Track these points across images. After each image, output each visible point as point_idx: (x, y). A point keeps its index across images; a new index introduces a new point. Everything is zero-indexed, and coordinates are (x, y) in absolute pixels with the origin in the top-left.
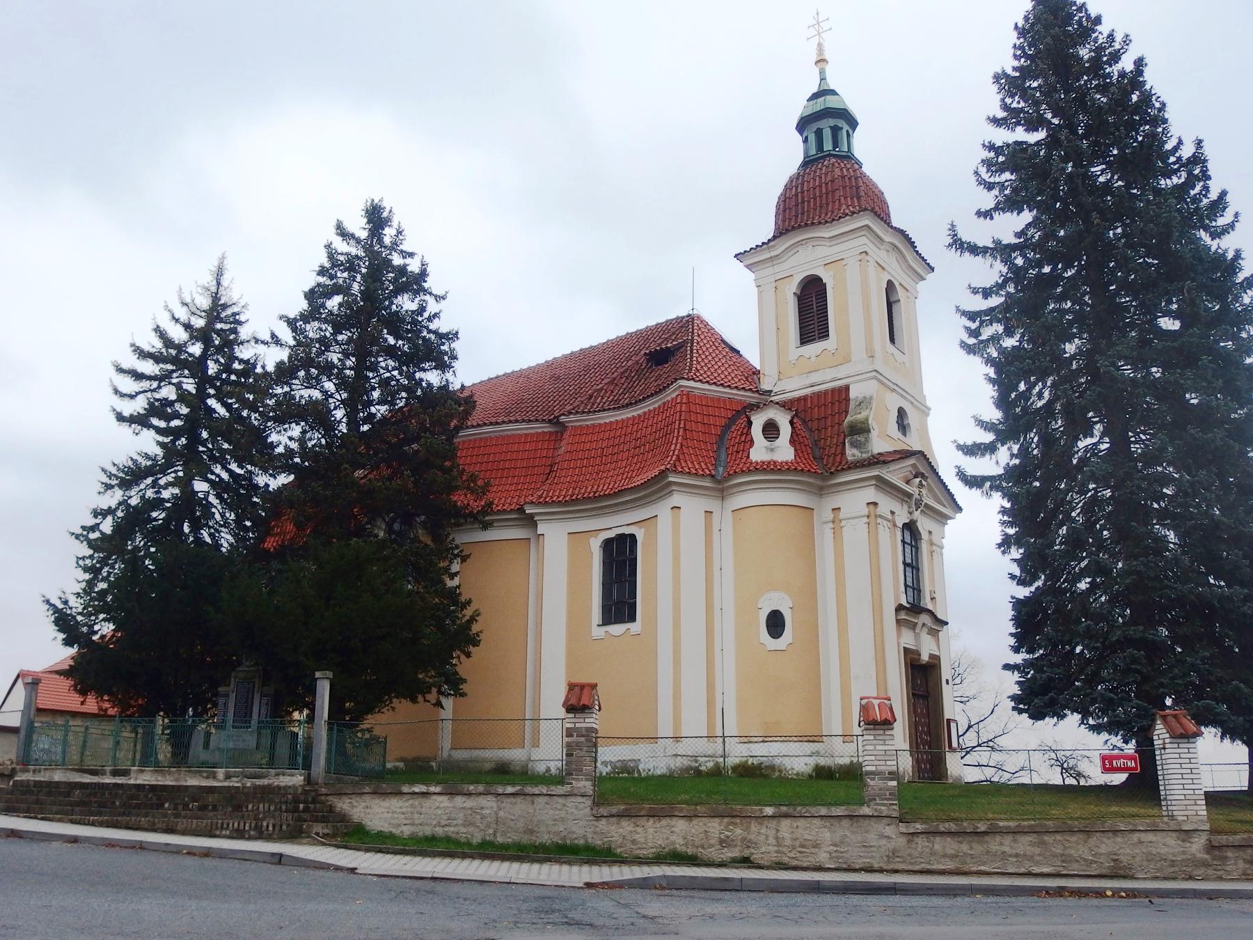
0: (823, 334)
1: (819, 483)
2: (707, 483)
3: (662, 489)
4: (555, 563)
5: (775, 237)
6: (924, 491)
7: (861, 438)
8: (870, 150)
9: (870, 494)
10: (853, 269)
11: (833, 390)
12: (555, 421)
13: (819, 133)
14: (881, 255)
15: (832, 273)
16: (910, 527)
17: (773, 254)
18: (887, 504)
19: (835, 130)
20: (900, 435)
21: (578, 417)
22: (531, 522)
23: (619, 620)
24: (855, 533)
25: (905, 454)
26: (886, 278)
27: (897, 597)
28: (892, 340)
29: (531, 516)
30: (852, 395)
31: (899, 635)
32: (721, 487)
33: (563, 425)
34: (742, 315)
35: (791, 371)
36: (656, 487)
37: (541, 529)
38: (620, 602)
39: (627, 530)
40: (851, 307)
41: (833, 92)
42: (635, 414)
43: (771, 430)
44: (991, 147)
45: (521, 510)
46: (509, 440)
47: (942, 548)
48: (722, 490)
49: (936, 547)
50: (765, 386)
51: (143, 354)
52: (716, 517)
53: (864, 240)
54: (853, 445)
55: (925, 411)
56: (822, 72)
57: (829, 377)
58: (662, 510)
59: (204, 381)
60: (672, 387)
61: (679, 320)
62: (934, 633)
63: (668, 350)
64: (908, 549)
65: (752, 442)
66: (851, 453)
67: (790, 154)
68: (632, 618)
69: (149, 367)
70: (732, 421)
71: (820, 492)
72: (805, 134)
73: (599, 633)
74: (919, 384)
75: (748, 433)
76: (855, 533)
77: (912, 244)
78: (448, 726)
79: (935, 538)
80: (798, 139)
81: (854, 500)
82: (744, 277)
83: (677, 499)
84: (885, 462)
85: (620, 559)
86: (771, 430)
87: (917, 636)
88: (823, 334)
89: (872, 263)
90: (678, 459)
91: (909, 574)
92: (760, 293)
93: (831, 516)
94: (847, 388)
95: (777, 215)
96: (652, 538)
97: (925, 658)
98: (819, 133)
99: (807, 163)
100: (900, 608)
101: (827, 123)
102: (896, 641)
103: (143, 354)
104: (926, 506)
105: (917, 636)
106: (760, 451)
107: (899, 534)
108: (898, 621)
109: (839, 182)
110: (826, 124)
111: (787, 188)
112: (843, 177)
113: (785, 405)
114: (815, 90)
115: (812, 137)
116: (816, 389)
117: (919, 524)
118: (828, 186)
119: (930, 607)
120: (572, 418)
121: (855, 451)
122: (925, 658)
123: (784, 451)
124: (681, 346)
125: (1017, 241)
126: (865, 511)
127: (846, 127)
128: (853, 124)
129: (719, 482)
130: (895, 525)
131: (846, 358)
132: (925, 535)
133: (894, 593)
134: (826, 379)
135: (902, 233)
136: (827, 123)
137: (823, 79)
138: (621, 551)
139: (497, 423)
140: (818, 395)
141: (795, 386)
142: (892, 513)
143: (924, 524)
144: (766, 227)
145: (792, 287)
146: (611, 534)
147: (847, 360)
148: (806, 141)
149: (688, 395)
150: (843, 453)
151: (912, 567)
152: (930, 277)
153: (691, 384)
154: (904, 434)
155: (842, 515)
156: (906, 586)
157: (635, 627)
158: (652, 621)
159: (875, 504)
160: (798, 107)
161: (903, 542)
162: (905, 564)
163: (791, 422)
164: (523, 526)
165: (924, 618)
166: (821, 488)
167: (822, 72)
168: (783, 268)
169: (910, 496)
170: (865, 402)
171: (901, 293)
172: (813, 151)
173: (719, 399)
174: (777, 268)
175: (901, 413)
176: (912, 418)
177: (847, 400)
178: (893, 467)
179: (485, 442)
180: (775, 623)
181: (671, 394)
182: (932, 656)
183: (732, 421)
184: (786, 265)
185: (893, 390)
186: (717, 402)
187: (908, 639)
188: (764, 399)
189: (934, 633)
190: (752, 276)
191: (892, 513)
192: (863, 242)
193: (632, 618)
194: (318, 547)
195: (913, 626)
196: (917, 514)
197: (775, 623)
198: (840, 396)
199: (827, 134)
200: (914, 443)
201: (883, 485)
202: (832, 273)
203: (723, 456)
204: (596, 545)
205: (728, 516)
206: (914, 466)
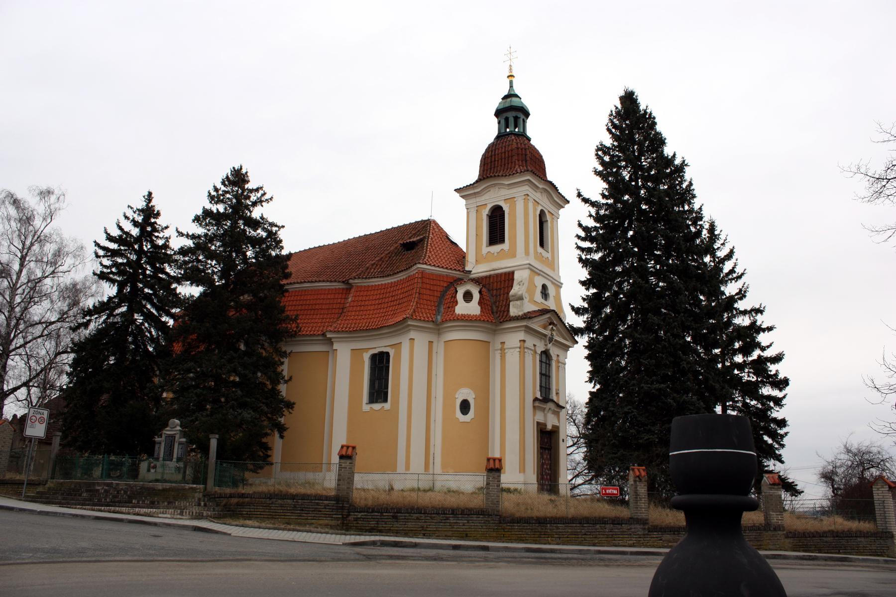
0: (502, 241)
1: (494, 327)
2: (430, 325)
3: (403, 328)
4: (344, 367)
5: (477, 182)
6: (554, 333)
8: (537, 132)
9: (521, 335)
12: (346, 282)
13: (507, 119)
14: (537, 196)
16: (546, 354)
18: (531, 341)
19: (516, 119)
20: (543, 301)
21: (360, 281)
22: (330, 342)
24: (513, 358)
25: (544, 312)
26: (539, 208)
27: (534, 393)
28: (542, 244)
29: (330, 339)
31: (534, 415)
32: (438, 328)
33: (350, 284)
34: (457, 223)
35: (482, 262)
36: (400, 327)
37: (335, 346)
38: (379, 390)
39: (385, 350)
40: (521, 226)
41: (516, 96)
43: (468, 296)
45: (324, 335)
46: (319, 292)
47: (565, 364)
48: (439, 330)
49: (562, 365)
51: (110, 238)
52: (435, 345)
53: (527, 188)
55: (558, 285)
56: (511, 82)
58: (405, 341)
59: (140, 253)
60: (415, 267)
61: (423, 222)
62: (557, 414)
63: (415, 240)
64: (544, 365)
65: (457, 303)
66: (514, 311)
67: (490, 130)
68: (385, 400)
69: (113, 246)
70: (448, 288)
71: (494, 332)
73: (366, 408)
75: (455, 297)
76: (513, 358)
77: (556, 188)
79: (561, 359)
80: (496, 120)
81: (513, 339)
82: (460, 203)
83: (413, 334)
84: (530, 318)
85: (381, 364)
87: (545, 416)
88: (502, 241)
89: (531, 200)
90: (414, 311)
91: (544, 380)
92: (468, 213)
93: (500, 346)
94: (513, 273)
95: (480, 166)
97: (549, 427)
98: (507, 119)
100: (536, 399)
101: (512, 113)
102: (532, 419)
103: (110, 238)
104: (556, 341)
105: (545, 416)
106: (463, 308)
107: (538, 357)
108: (534, 407)
110: (511, 115)
111: (487, 150)
112: (518, 148)
113: (477, 281)
114: (506, 93)
115: (503, 122)
116: (492, 273)
117: (551, 352)
118: (511, 154)
119: (555, 399)
120: (356, 281)
122: (549, 427)
123: (472, 308)
124: (422, 240)
125: (604, 201)
126: (519, 345)
127: (522, 117)
128: (527, 114)
129: (437, 325)
130: (535, 352)
131: (516, 256)
132: (554, 358)
133: (533, 390)
134: (502, 265)
135: (551, 183)
136: (512, 113)
137: (511, 86)
138: (381, 361)
139: (312, 282)
142: (535, 345)
143: (554, 351)
144: (472, 174)
145: (486, 212)
146: (376, 351)
148: (499, 123)
149: (423, 273)
150: (508, 311)
151: (545, 377)
152: (567, 206)
153: (424, 266)
154: (546, 300)
155: (505, 347)
156: (541, 386)
157: (387, 406)
159: (524, 341)
160: (496, 102)
161: (541, 361)
162: (541, 374)
163: (480, 292)
164: (324, 344)
165: (550, 405)
166: (495, 331)
167: (511, 82)
168: (481, 200)
169: (545, 336)
171: (548, 217)
173: (440, 275)
174: (478, 199)
175: (544, 287)
176: (551, 290)
177: (513, 279)
178: (536, 320)
179: (305, 292)
180: (465, 407)
181: (413, 271)
182: (553, 426)
183: (448, 288)
184: (483, 198)
185: (539, 275)
186: (439, 277)
187: (540, 417)
188: (464, 277)
189: (557, 414)
190: (463, 201)
191: (535, 345)
192: (526, 189)
193: (385, 400)
194: (206, 344)
195: (543, 410)
196: (550, 346)
200: (551, 304)
201: (529, 330)
203: (442, 310)
204: (367, 357)
205: (442, 345)
206: (549, 318)
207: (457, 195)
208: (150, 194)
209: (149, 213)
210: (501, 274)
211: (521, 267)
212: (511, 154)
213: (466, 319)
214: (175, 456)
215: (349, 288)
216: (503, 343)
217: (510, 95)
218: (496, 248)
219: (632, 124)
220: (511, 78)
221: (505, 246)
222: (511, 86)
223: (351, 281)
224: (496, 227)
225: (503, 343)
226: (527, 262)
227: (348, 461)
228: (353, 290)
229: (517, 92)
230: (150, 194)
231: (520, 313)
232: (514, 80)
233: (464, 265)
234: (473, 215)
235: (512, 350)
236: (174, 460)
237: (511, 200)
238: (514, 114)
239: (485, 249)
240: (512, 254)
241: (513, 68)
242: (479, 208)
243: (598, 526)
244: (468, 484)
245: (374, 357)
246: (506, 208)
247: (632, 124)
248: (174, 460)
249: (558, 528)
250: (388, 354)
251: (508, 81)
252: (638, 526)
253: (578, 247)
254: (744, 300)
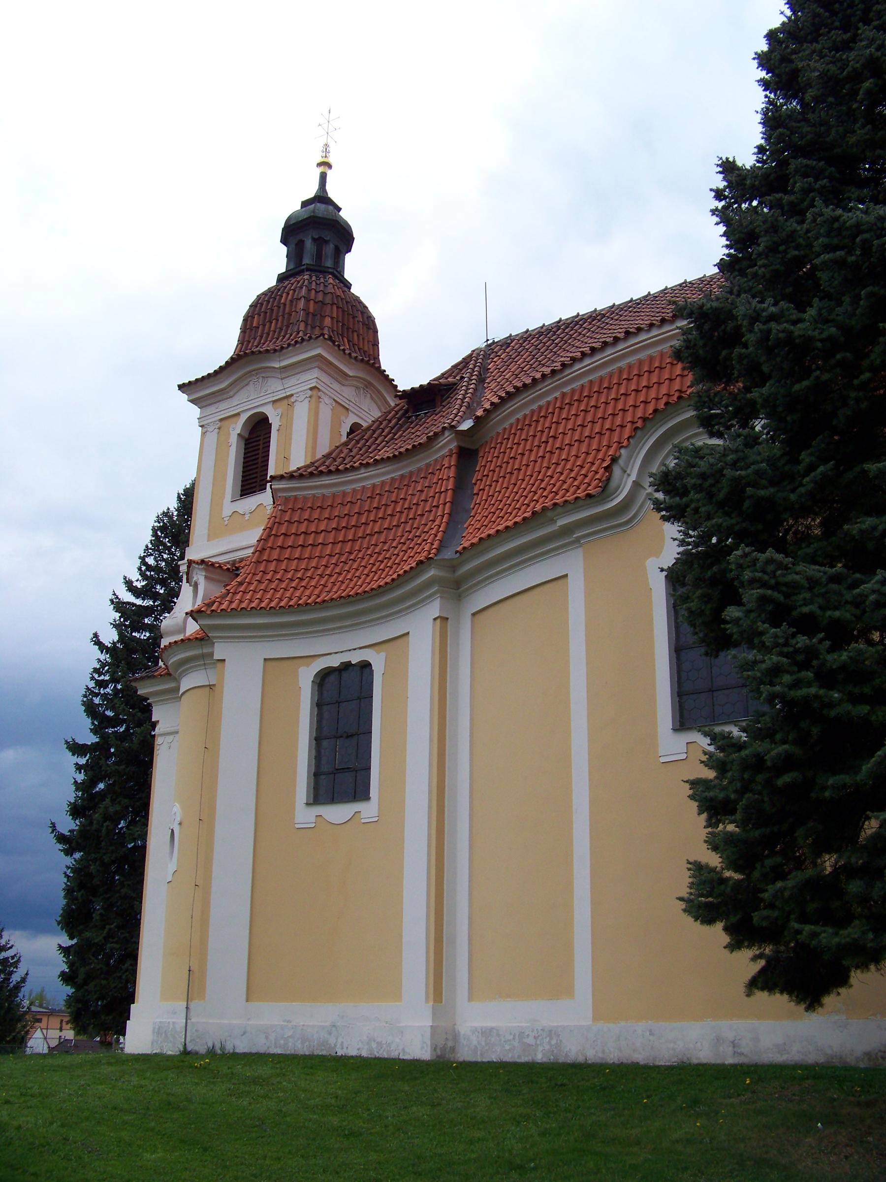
10: (302, 411)
14: (348, 393)
15: (279, 411)
38: (342, 765)
39: (355, 658)
56: (323, 178)
68: (366, 797)
73: (305, 815)
82: (190, 412)
85: (344, 701)
92: (204, 434)
101: (318, 235)
111: (253, 306)
136: (318, 235)
145: (237, 428)
146: (335, 662)
157: (368, 810)
167: (323, 178)
168: (226, 408)
174: (223, 405)
184: (235, 401)
190: (195, 411)
193: (366, 797)
204: (306, 676)
217: (322, 198)
232: (330, 174)
234: (212, 437)
238: (327, 235)
241: (331, 149)
245: (323, 678)
251: (318, 171)
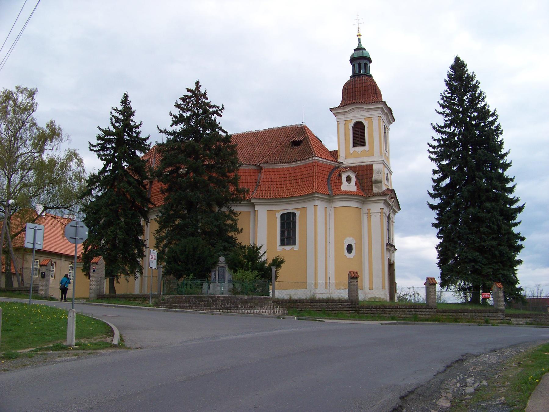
0: (363, 144)
2: (326, 197)
7: (379, 185)
8: (376, 71)
9: (382, 205)
11: (367, 165)
13: (360, 65)
17: (345, 110)
19: (366, 64)
22: (253, 205)
23: (288, 244)
29: (253, 203)
30: (375, 167)
33: (261, 167)
34: (331, 135)
35: (351, 157)
36: (310, 196)
37: (256, 208)
41: (364, 49)
42: (292, 166)
43: (349, 179)
44: (501, 133)
50: (340, 160)
52: (328, 209)
54: (376, 187)
56: (359, 39)
57: (365, 161)
58: (310, 206)
66: (375, 190)
67: (346, 72)
68: (294, 244)
71: (363, 202)
72: (353, 64)
73: (280, 248)
74: (389, 164)
77: (391, 112)
78: (146, 278)
80: (350, 67)
81: (377, 207)
83: (317, 202)
86: (349, 179)
88: (363, 144)
92: (338, 124)
96: (304, 215)
98: (360, 65)
99: (354, 76)
101: (360, 61)
106: (346, 187)
109: (370, 87)
110: (363, 62)
113: (353, 169)
114: (356, 47)
115: (357, 66)
118: (361, 88)
120: (265, 165)
121: (376, 189)
126: (380, 211)
128: (370, 61)
133: (386, 241)
134: (364, 160)
135: (390, 110)
136: (360, 61)
137: (360, 42)
140: (361, 166)
141: (351, 162)
144: (337, 99)
145: (351, 125)
146: (285, 212)
147: (372, 155)
149: (317, 162)
150: (372, 189)
152: (393, 123)
155: (371, 212)
157: (296, 247)
158: (304, 246)
163: (356, 176)
167: (359, 39)
170: (379, 172)
172: (357, 72)
174: (346, 116)
177: (372, 169)
180: (350, 248)
193: (294, 244)
197: (350, 248)
198: (369, 168)
199: (363, 65)
202: (367, 122)
205: (333, 209)
207: (331, 113)
208: (126, 96)
209: (127, 112)
210: (364, 166)
211: (377, 162)
212: (361, 88)
213: (349, 194)
214: (226, 279)
215: (260, 169)
216: (369, 209)
217: (359, 49)
218: (359, 149)
219: (460, 81)
220: (359, 37)
221: (366, 148)
222: (360, 42)
223: (261, 165)
224: (359, 135)
225: (369, 209)
226: (382, 159)
227: (356, 280)
228: (263, 171)
229: (363, 46)
230: (126, 96)
231: (380, 191)
232: (361, 37)
233: (337, 159)
234: (342, 126)
235: (376, 214)
236: (226, 281)
237: (369, 119)
238: (365, 61)
239: (352, 149)
240: (371, 153)
242: (346, 122)
243: (482, 314)
244: (343, 294)
246: (365, 123)
247: (460, 81)
248: (226, 281)
249: (464, 315)
250: (294, 214)
251: (357, 38)
252: (501, 314)
253: (430, 152)
254: (77, 152)
